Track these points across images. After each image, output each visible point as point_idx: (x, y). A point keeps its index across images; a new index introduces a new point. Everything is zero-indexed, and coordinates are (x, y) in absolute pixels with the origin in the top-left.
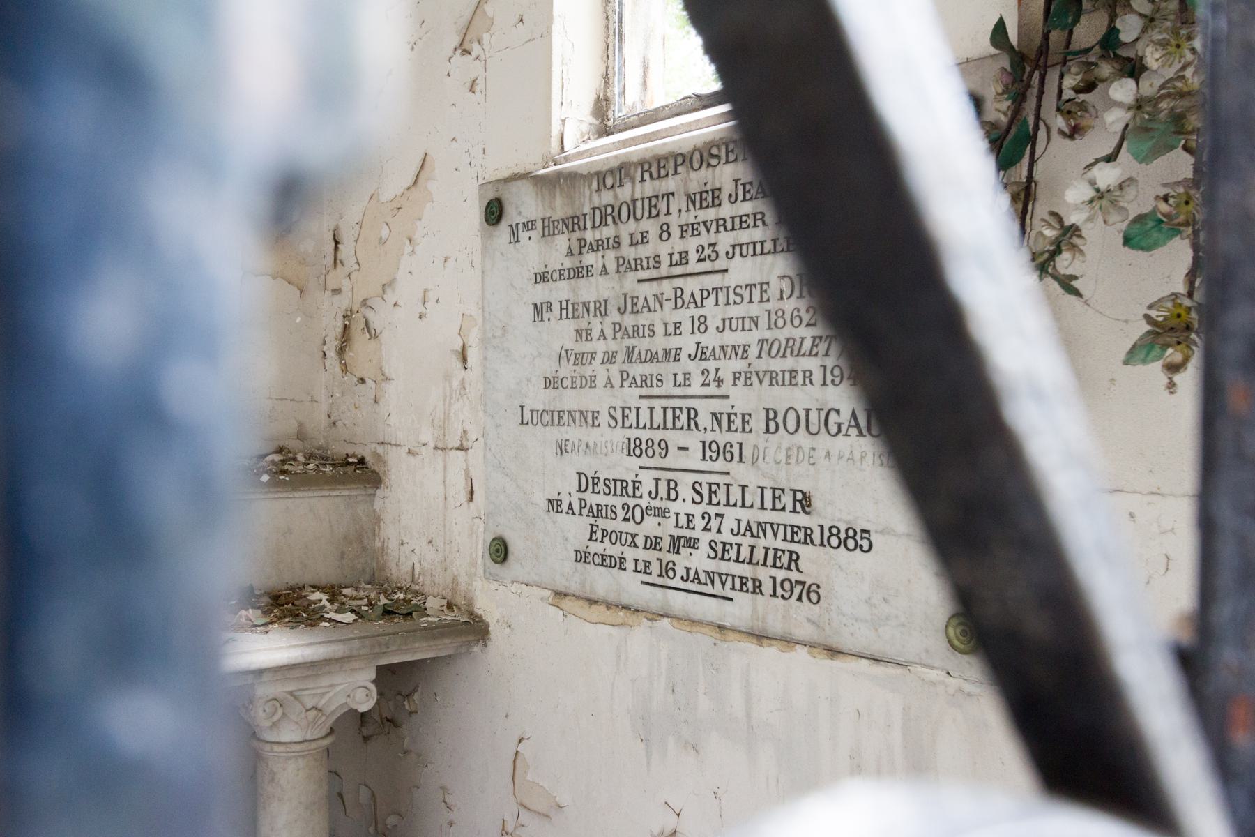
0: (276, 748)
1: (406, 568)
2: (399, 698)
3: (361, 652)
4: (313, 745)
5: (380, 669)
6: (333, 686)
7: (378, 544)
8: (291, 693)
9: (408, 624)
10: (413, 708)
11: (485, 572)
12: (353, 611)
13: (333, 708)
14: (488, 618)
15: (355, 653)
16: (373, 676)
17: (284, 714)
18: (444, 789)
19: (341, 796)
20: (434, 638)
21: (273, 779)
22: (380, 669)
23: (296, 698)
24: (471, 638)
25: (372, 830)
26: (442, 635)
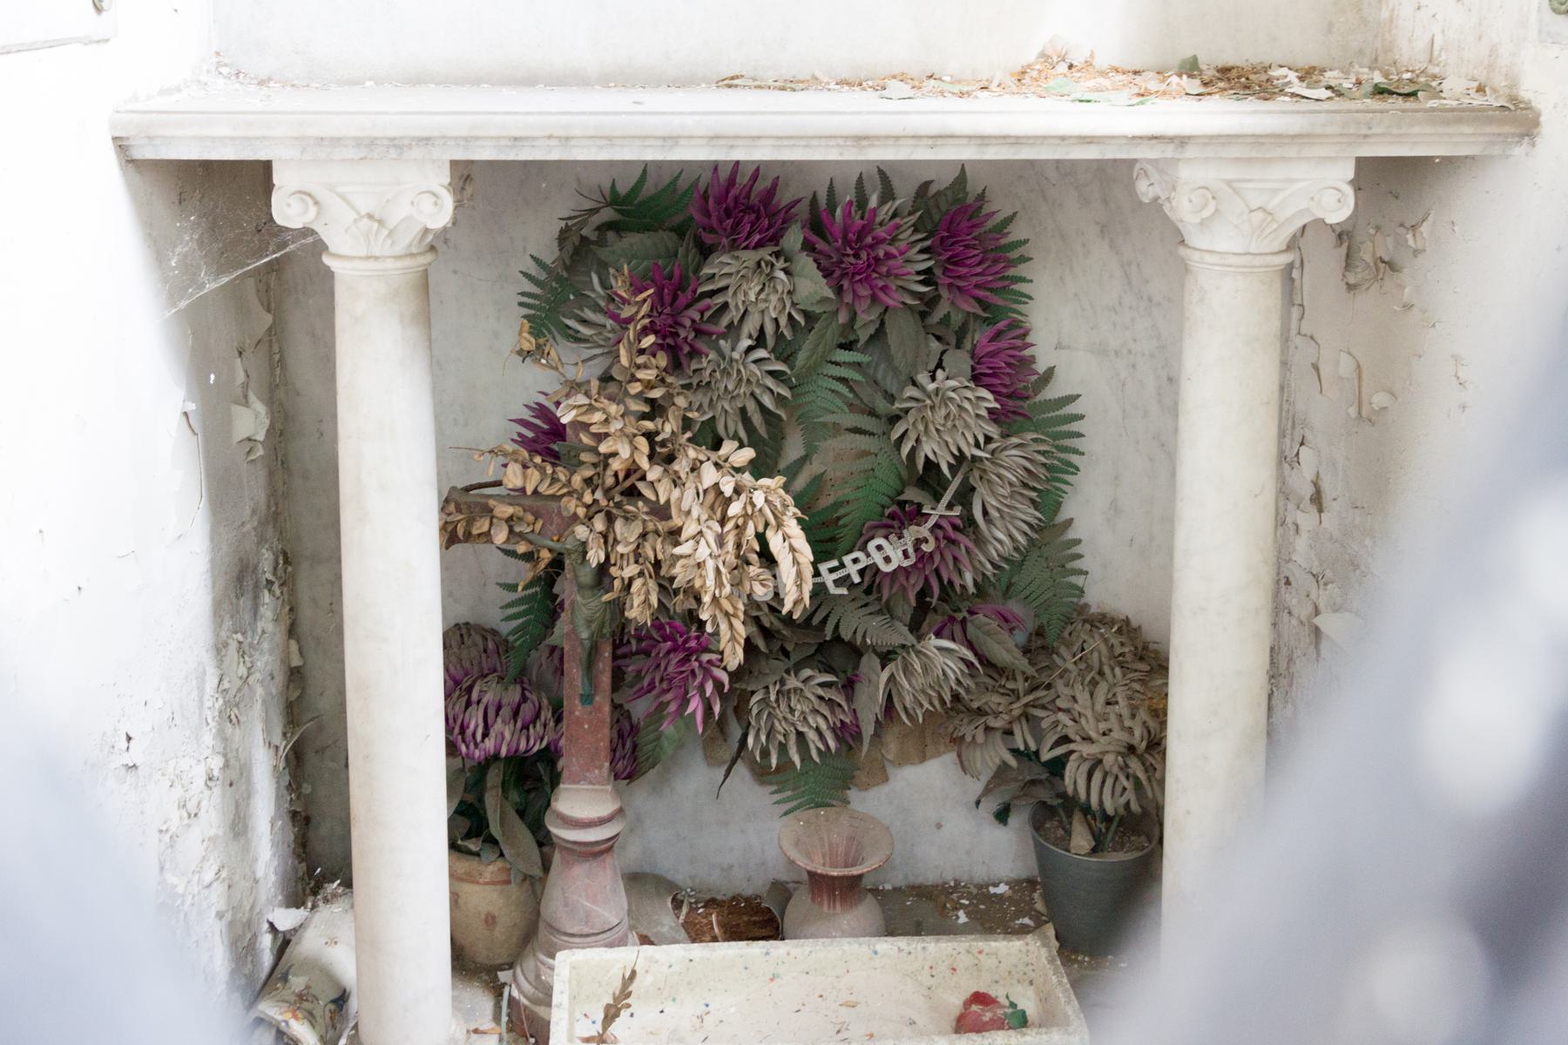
0: (1207, 258)
1: (1421, 45)
2: (1401, 230)
3: (1328, 130)
4: (1258, 261)
5: (1360, 161)
6: (1291, 181)
7: (1385, 14)
8: (1229, 183)
9: (1410, 104)
10: (1420, 246)
11: (1540, 32)
12: (1329, 88)
13: (1289, 213)
14: (1539, 103)
15: (1318, 130)
16: (1351, 175)
17: (1217, 210)
18: (1457, 359)
19: (1316, 367)
20: (1447, 123)
21: (1202, 300)
22: (1360, 161)
23: (1236, 191)
24: (1507, 129)
25: (1353, 411)
26: (1459, 121)
